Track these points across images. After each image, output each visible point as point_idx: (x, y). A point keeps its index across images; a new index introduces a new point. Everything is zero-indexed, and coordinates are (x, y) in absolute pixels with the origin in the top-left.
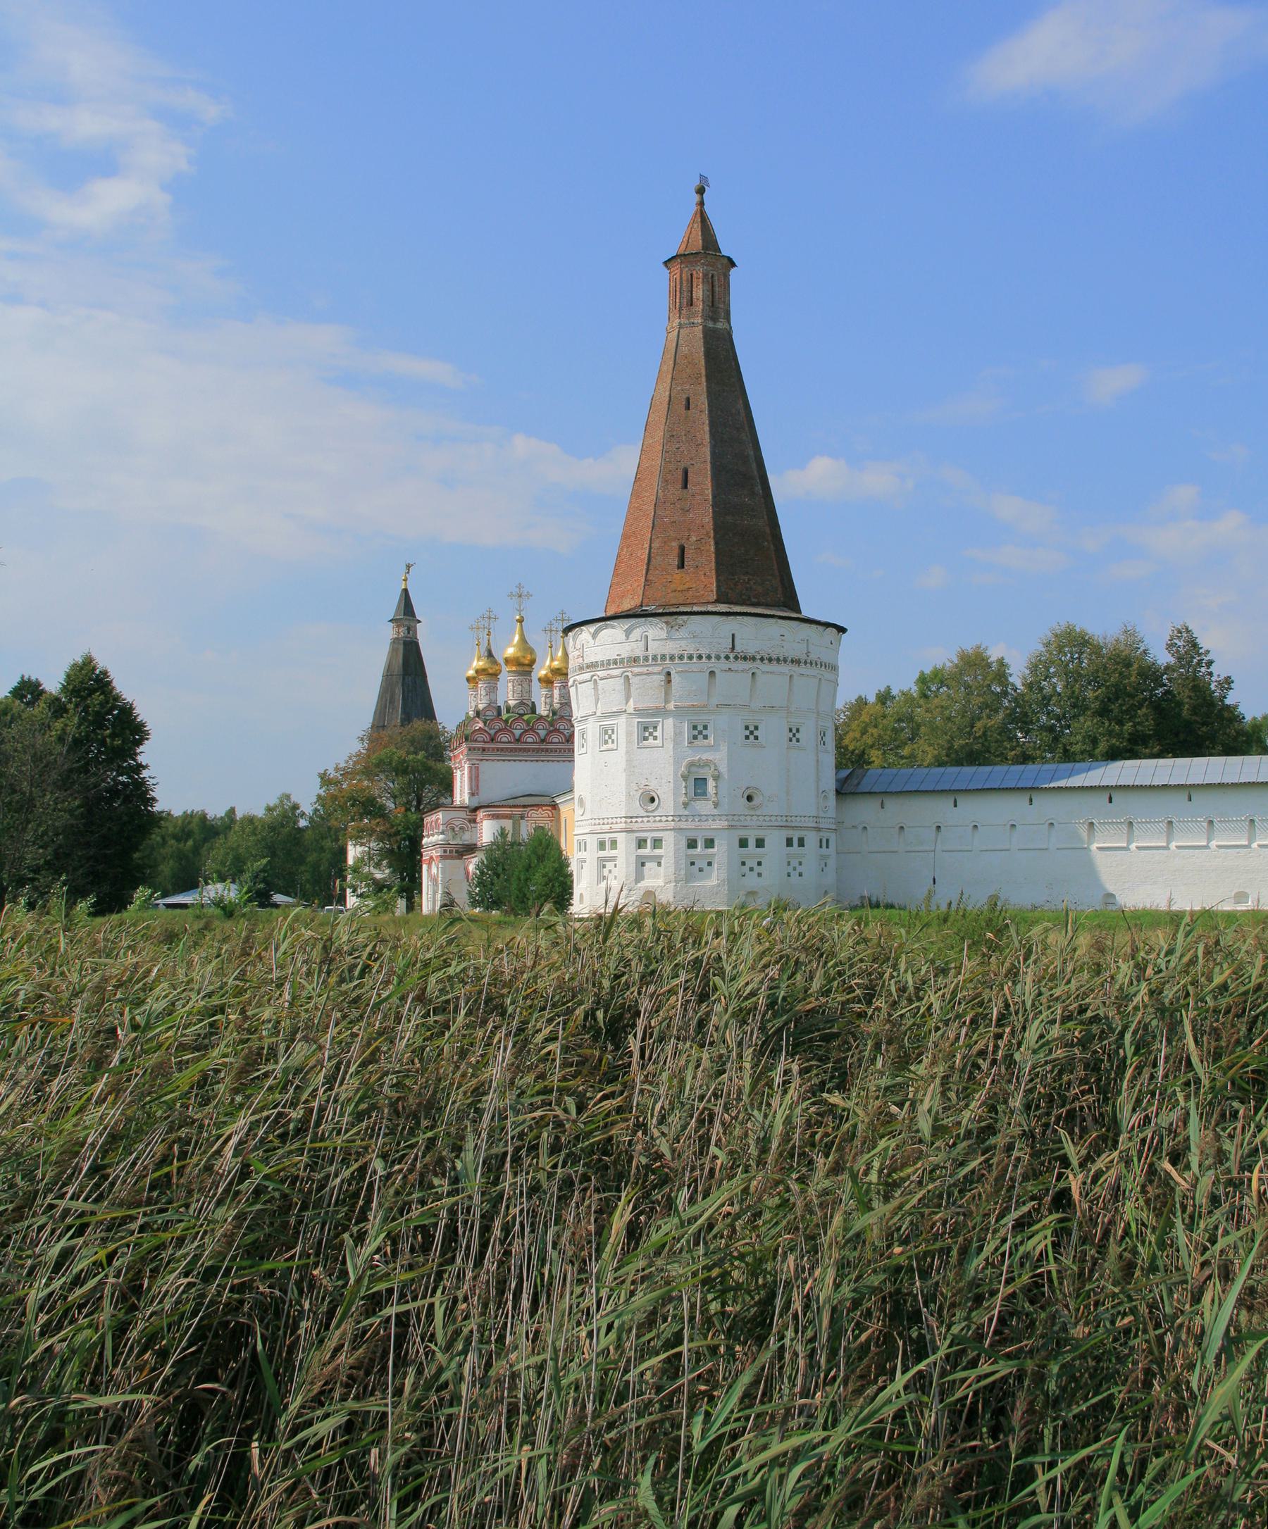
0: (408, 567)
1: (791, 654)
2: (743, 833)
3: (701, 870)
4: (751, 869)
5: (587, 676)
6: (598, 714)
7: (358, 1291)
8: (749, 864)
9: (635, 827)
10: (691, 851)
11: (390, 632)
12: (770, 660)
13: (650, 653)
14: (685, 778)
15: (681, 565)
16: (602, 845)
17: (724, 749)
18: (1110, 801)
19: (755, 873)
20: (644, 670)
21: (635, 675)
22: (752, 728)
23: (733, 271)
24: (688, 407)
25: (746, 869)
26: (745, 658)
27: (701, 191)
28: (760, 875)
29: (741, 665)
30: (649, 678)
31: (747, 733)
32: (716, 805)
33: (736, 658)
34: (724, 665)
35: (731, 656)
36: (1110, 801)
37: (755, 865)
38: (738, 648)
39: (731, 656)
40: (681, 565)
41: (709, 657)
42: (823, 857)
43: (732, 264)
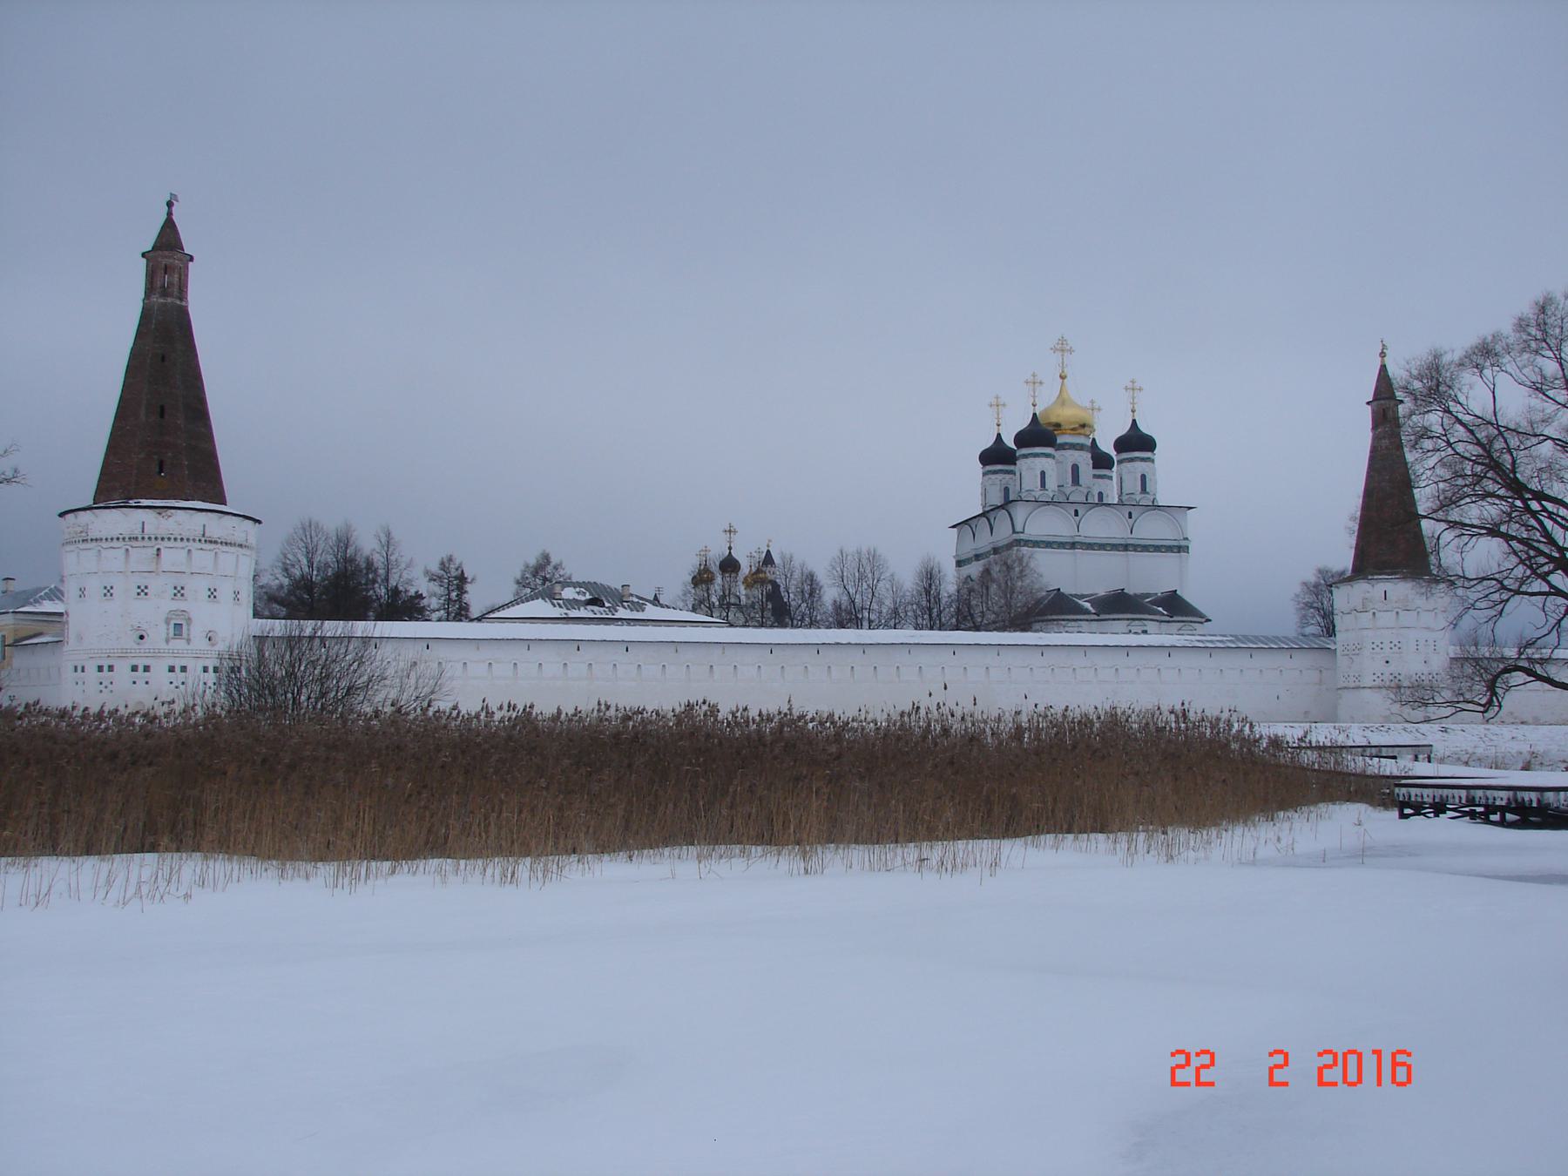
1: (239, 541)
2: (135, 662)
4: (1395, 645)
8: (175, 684)
12: (226, 544)
18: (998, 655)
22: (179, 588)
23: (190, 263)
26: (211, 542)
27: (170, 204)
31: (142, 588)
33: (206, 541)
34: (198, 545)
35: (203, 539)
36: (998, 655)
37: (1380, 675)
38: (206, 535)
39: (203, 539)
43: (191, 259)
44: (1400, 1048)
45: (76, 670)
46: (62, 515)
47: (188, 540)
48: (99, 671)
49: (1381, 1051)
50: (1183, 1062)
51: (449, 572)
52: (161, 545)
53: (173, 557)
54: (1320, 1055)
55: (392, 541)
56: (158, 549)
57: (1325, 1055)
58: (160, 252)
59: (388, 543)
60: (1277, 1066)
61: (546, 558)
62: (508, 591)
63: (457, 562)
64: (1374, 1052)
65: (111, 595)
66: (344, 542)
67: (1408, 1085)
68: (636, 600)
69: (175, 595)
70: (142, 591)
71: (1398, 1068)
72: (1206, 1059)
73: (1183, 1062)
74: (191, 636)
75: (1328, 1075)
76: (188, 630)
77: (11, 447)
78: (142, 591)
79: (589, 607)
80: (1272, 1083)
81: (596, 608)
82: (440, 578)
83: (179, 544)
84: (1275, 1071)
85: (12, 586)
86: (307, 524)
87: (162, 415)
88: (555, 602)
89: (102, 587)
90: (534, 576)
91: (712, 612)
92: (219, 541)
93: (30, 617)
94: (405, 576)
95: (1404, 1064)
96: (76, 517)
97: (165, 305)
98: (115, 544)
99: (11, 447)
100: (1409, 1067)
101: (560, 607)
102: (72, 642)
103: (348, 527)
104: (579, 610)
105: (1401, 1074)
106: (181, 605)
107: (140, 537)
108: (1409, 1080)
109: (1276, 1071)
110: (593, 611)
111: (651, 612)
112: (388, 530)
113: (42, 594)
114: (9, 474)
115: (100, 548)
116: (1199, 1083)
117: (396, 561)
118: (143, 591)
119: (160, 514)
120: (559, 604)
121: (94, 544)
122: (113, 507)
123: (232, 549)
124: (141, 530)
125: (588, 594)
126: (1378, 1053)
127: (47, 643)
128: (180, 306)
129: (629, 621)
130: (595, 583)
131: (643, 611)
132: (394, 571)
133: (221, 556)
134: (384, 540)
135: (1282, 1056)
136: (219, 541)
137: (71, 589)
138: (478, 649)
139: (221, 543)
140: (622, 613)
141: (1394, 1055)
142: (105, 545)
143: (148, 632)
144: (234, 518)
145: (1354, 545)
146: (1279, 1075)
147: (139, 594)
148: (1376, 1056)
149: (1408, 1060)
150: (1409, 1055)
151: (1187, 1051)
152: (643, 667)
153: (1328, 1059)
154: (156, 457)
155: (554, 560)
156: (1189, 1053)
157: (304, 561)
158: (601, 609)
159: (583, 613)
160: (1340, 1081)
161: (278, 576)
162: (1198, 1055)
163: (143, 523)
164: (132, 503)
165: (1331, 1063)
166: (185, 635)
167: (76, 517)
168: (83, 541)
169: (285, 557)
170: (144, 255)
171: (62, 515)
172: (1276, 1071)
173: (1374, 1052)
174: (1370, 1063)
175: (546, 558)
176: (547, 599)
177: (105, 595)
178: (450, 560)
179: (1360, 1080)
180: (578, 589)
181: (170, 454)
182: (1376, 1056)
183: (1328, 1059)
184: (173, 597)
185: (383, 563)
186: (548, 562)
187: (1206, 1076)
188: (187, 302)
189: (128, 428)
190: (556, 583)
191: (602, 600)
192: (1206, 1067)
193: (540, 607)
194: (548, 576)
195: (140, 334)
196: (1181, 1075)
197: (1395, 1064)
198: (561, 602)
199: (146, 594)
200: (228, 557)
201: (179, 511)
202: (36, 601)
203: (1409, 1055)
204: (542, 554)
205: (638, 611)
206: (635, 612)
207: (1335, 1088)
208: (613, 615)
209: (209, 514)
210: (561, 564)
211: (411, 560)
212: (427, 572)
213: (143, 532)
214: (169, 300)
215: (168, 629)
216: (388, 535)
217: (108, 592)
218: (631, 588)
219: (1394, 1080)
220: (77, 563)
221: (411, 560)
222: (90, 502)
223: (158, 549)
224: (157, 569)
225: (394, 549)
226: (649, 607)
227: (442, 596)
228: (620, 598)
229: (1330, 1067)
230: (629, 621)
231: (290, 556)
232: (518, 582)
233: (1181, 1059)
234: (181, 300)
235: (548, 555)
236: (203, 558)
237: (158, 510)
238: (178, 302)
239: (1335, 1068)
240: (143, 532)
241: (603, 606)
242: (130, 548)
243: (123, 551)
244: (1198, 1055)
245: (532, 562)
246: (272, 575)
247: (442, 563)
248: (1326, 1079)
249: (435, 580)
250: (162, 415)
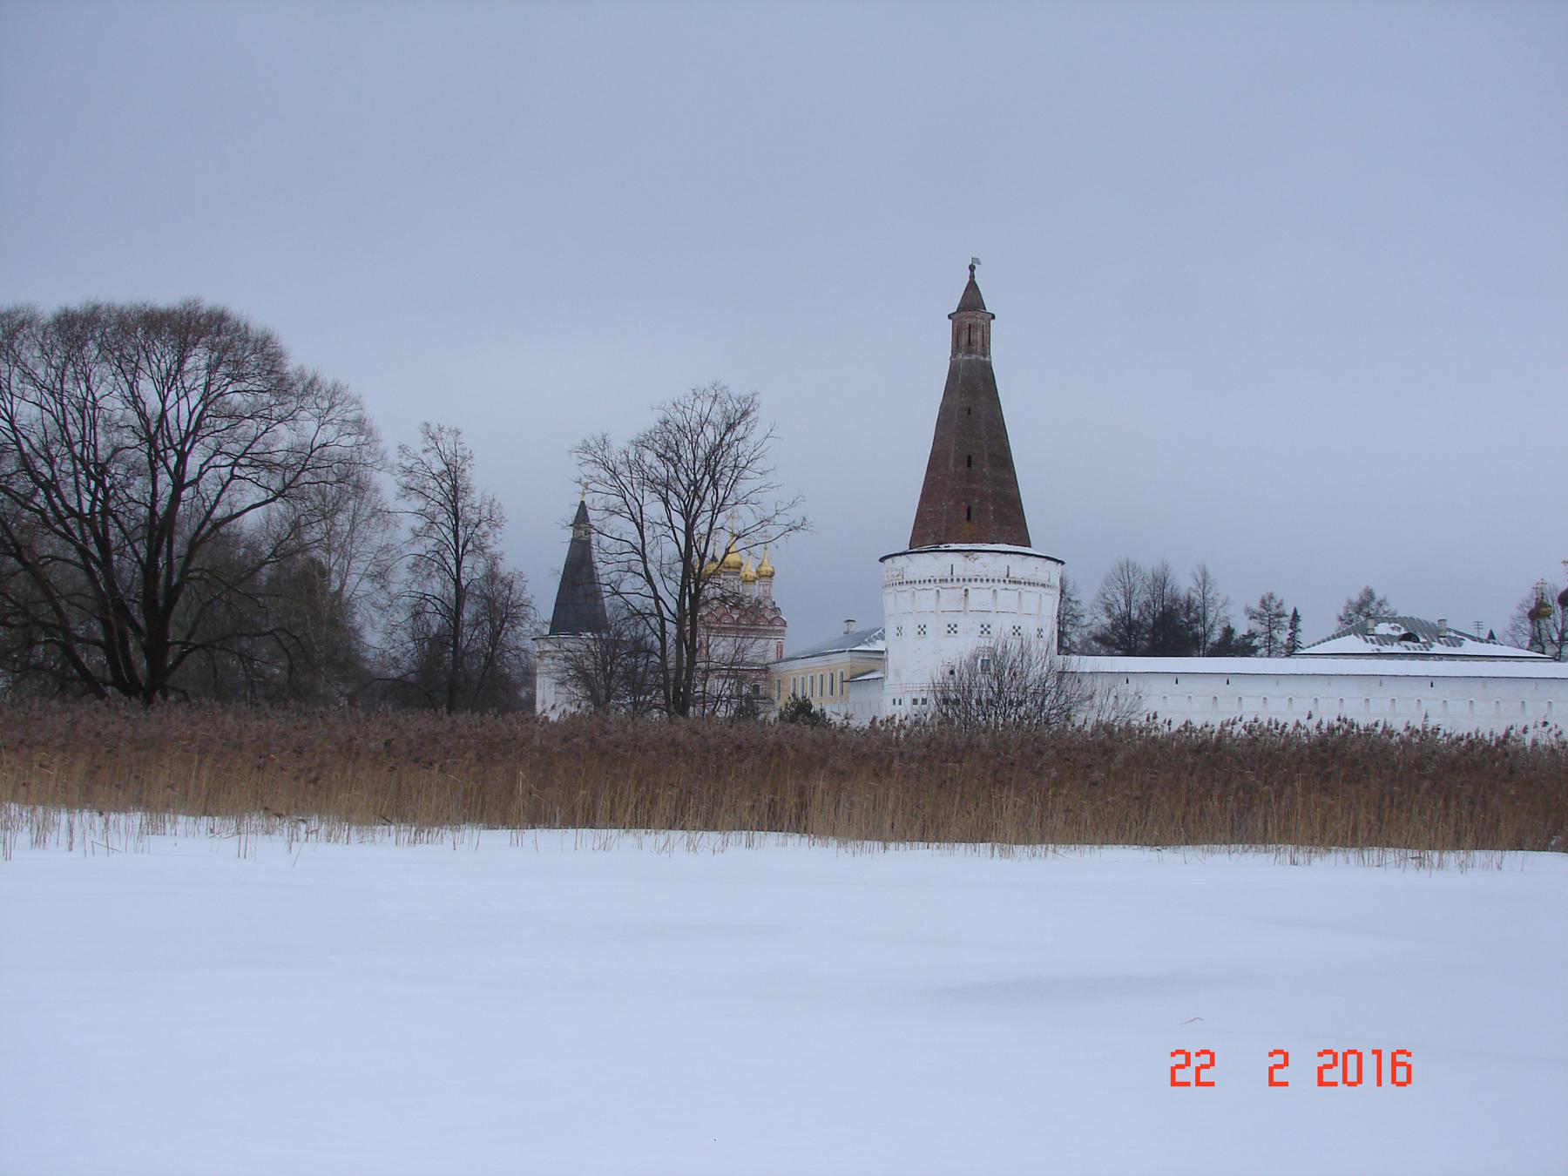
7: (691, 634)
12: (1029, 584)
15: (969, 518)
17: (609, 611)
23: (992, 321)
24: (969, 413)
26: (1015, 582)
27: (972, 268)
29: (1013, 586)
30: (953, 591)
31: (952, 626)
33: (1010, 581)
34: (1002, 585)
35: (1007, 580)
38: (1011, 575)
39: (1007, 580)
40: (969, 518)
43: (950, 317)
44: (1400, 1048)
45: (900, 701)
46: (882, 560)
47: (993, 580)
49: (1381, 1051)
50: (1183, 1062)
51: (1270, 610)
52: (969, 586)
53: (980, 597)
54: (1320, 1055)
55: (1208, 580)
56: (966, 590)
57: (1325, 1055)
58: (964, 313)
59: (1204, 581)
60: (1277, 1066)
61: (1370, 594)
62: (1333, 626)
63: (1278, 599)
64: (1374, 1052)
65: (925, 633)
66: (1160, 582)
67: (1408, 1085)
68: (1453, 635)
69: (982, 633)
70: (952, 629)
71: (1398, 1068)
72: (1205, 1059)
73: (1183, 1062)
75: (1328, 1075)
77: (797, 498)
78: (952, 629)
79: (1404, 643)
80: (1272, 1083)
81: (1410, 644)
82: (1261, 615)
83: (985, 585)
84: (1177, 1071)
85: (854, 628)
86: (1125, 565)
87: (969, 465)
88: (1368, 637)
89: (946, 625)
90: (1357, 612)
91: (1544, 647)
92: (1023, 581)
93: (858, 655)
94: (1222, 614)
95: (1404, 1064)
96: (893, 562)
97: (970, 361)
98: (927, 585)
99: (797, 498)
100: (1409, 1067)
101: (1373, 642)
102: (891, 679)
103: (1165, 567)
104: (1392, 645)
105: (1401, 1074)
107: (949, 579)
108: (1409, 1081)
109: (1276, 1071)
110: (1406, 646)
111: (1469, 647)
112: (1204, 568)
113: (876, 634)
114: (798, 523)
115: (939, 588)
116: (1199, 1083)
117: (1213, 598)
118: (952, 629)
119: (967, 557)
120: (1371, 640)
121: (909, 586)
122: (925, 552)
123: (1036, 589)
125: (1403, 629)
126: (1378, 1053)
127: (877, 679)
128: (985, 362)
129: (1441, 656)
130: (1411, 618)
131: (1460, 646)
132: (1211, 608)
133: (1025, 595)
134: (1200, 578)
135: (1282, 1056)
136: (1023, 581)
137: (891, 631)
138: (1277, 684)
139: (1025, 583)
140: (1438, 648)
141: (1394, 1055)
142: (918, 586)
144: (1036, 559)
146: (1279, 1075)
147: (949, 632)
148: (1375, 1056)
149: (1408, 1060)
150: (1409, 1055)
151: (1187, 1051)
152: (1449, 703)
153: (1328, 1059)
154: (964, 504)
155: (1378, 596)
156: (1337, 1053)
157: (1122, 601)
158: (1416, 645)
159: (1396, 648)
160: (1340, 1081)
161: (1097, 615)
162: (1198, 1055)
163: (1008, 567)
164: (942, 547)
165: (1209, 1063)
167: (893, 562)
168: (900, 583)
169: (1105, 597)
170: (950, 317)
171: (882, 560)
172: (1276, 1071)
173: (1374, 1052)
174: (1370, 1063)
175: (1370, 594)
176: (1359, 635)
177: (919, 633)
178: (1271, 597)
179: (1360, 1080)
180: (1393, 625)
181: (977, 501)
182: (1375, 1056)
183: (1328, 1059)
184: (979, 634)
185: (1199, 601)
186: (1372, 598)
187: (1205, 1076)
188: (990, 357)
189: (939, 477)
191: (1416, 636)
192: (1207, 1067)
193: (1353, 643)
194: (1371, 612)
195: (948, 390)
196: (1181, 1075)
197: (1395, 1064)
198: (1374, 638)
200: (1031, 597)
201: (984, 554)
202: (871, 641)
203: (1409, 1055)
204: (1365, 590)
205: (1455, 646)
206: (1452, 647)
207: (1285, 1088)
208: (1428, 650)
209: (1013, 555)
210: (1385, 600)
211: (1227, 599)
212: (1248, 610)
213: (952, 573)
214: (973, 357)
216: (1205, 574)
217: (922, 630)
218: (1447, 623)
219: (1394, 1080)
220: (896, 604)
221: (1227, 599)
222: (906, 548)
223: (966, 590)
224: (965, 608)
225: (1210, 588)
226: (1467, 642)
227: (1263, 633)
228: (1436, 633)
229: (1330, 1067)
230: (1441, 656)
231: (1109, 596)
232: (1341, 619)
233: (1181, 1059)
234: (985, 356)
235: (1371, 590)
236: (1008, 597)
237: (967, 553)
238: (982, 358)
239: (1335, 1068)
240: (952, 573)
241: (1418, 641)
242: (940, 590)
243: (934, 592)
244: (1198, 1055)
245: (1356, 598)
246: (1091, 614)
247: (1263, 601)
248: (1326, 1079)
249: (1255, 618)
250: (969, 465)
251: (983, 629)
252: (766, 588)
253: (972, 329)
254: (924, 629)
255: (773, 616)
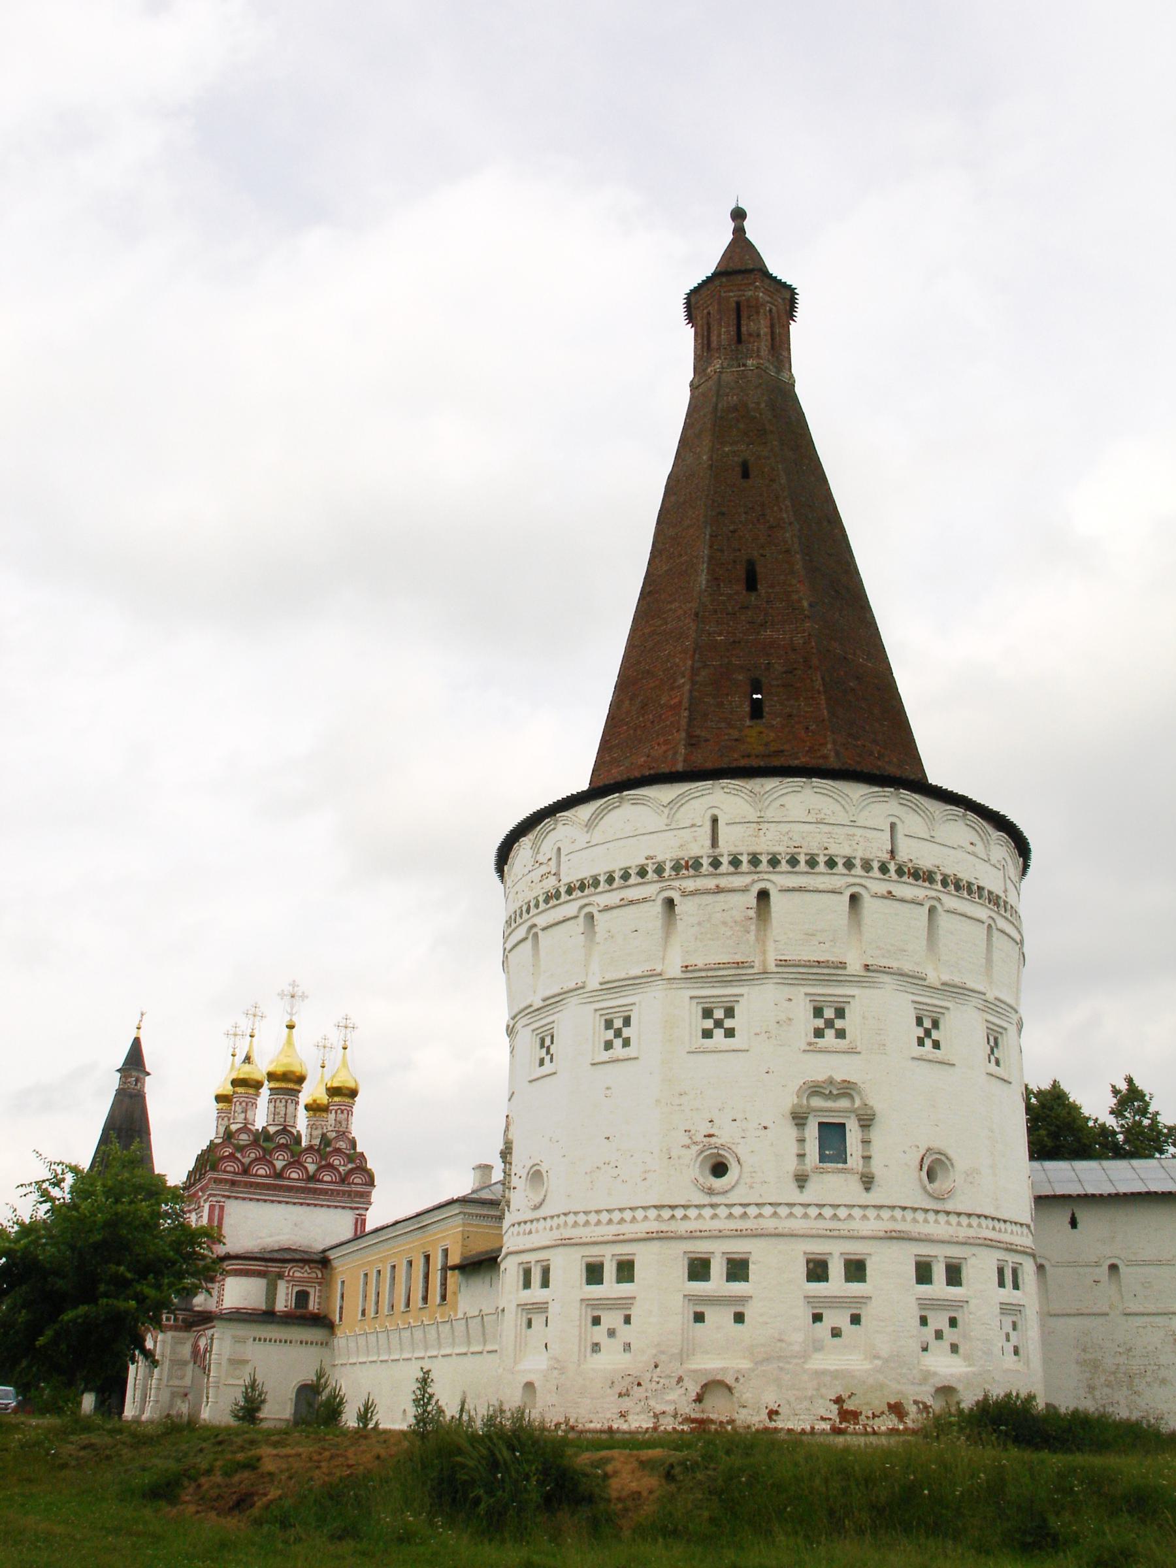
0: (142, 1015)
3: (836, 1333)
5: (570, 909)
6: (593, 984)
9: (682, 1227)
10: (699, 1287)
11: (113, 1082)
13: (726, 846)
14: (799, 1119)
16: (594, 1273)
18: (1074, 1223)
19: (945, 1345)
20: (711, 883)
21: (684, 894)
25: (929, 1331)
26: (916, 874)
28: (954, 1348)
32: (868, 1182)
35: (892, 867)
36: (1074, 1223)
37: (944, 1325)
39: (892, 867)
41: (849, 864)
42: (1007, 1309)
45: (546, 1272)
48: (590, 1282)
52: (776, 881)
74: (876, 1167)
76: (866, 1142)
106: (839, 1068)
124: (708, 843)
143: (739, 1151)
145: (744, 576)
166: (854, 1159)
190: (576, 917)
199: (730, 1033)
213: (714, 843)
215: (802, 1141)
223: (763, 895)
243: (658, 908)
251: (820, 1023)
252: (341, 1117)
253: (744, 315)
254: (626, 1032)
255: (350, 1166)
